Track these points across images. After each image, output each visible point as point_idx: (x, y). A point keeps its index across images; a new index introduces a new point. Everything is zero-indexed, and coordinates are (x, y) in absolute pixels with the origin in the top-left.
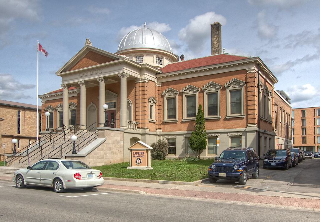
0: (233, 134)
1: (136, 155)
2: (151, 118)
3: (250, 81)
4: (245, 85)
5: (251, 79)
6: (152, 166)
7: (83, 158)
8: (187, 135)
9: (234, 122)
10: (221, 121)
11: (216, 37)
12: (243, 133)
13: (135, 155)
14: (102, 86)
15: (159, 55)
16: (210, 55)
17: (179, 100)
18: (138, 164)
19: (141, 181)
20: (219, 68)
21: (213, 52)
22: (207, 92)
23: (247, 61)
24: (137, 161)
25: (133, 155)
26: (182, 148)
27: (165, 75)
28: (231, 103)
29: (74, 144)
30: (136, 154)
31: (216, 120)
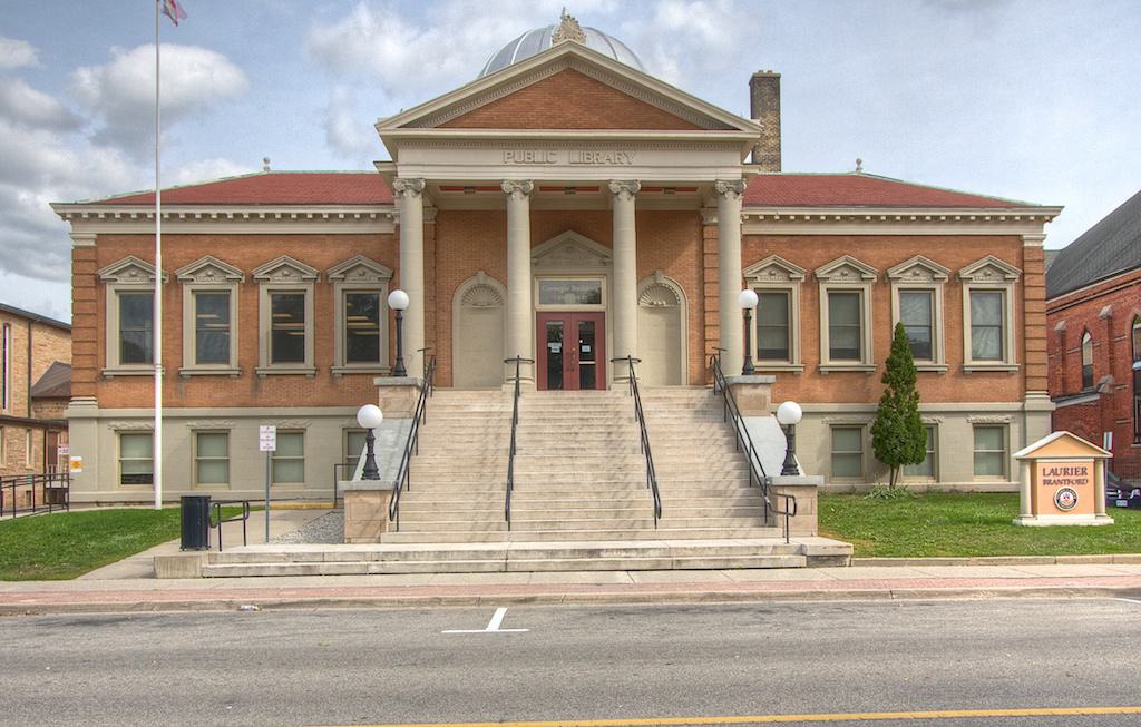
0: (985, 418)
1: (1056, 478)
3: (1031, 271)
4: (1017, 281)
5: (1034, 265)
8: (839, 417)
9: (985, 382)
10: (948, 378)
12: (1013, 415)
13: (1052, 478)
14: (626, 212)
17: (804, 299)
18: (1059, 506)
19: (1045, 562)
20: (268, 216)
22: (270, 287)
23: (1032, 214)
24: (1062, 497)
26: (818, 459)
30: (1056, 474)
31: (984, 374)
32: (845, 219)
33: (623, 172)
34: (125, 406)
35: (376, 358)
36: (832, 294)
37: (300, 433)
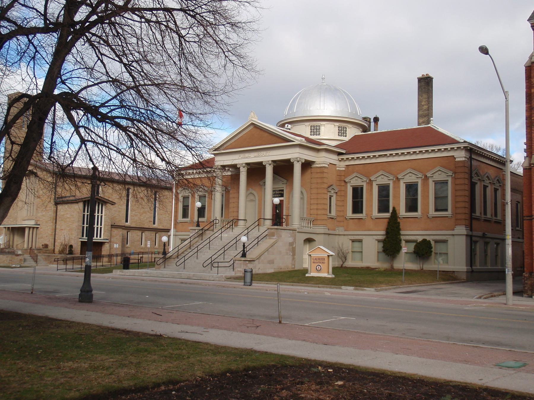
2: (330, 212)
6: (333, 273)
7: (253, 262)
11: (425, 96)
13: (315, 261)
15: (342, 123)
16: (416, 126)
18: (318, 271)
21: (419, 124)
25: (312, 261)
27: (350, 156)
28: (436, 198)
29: (244, 246)
32: (380, 156)
33: (268, 157)
34: (182, 232)
35: (361, 212)
36: (436, 183)
37: (360, 241)
